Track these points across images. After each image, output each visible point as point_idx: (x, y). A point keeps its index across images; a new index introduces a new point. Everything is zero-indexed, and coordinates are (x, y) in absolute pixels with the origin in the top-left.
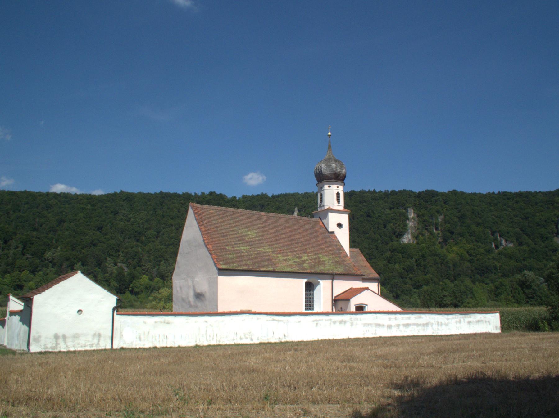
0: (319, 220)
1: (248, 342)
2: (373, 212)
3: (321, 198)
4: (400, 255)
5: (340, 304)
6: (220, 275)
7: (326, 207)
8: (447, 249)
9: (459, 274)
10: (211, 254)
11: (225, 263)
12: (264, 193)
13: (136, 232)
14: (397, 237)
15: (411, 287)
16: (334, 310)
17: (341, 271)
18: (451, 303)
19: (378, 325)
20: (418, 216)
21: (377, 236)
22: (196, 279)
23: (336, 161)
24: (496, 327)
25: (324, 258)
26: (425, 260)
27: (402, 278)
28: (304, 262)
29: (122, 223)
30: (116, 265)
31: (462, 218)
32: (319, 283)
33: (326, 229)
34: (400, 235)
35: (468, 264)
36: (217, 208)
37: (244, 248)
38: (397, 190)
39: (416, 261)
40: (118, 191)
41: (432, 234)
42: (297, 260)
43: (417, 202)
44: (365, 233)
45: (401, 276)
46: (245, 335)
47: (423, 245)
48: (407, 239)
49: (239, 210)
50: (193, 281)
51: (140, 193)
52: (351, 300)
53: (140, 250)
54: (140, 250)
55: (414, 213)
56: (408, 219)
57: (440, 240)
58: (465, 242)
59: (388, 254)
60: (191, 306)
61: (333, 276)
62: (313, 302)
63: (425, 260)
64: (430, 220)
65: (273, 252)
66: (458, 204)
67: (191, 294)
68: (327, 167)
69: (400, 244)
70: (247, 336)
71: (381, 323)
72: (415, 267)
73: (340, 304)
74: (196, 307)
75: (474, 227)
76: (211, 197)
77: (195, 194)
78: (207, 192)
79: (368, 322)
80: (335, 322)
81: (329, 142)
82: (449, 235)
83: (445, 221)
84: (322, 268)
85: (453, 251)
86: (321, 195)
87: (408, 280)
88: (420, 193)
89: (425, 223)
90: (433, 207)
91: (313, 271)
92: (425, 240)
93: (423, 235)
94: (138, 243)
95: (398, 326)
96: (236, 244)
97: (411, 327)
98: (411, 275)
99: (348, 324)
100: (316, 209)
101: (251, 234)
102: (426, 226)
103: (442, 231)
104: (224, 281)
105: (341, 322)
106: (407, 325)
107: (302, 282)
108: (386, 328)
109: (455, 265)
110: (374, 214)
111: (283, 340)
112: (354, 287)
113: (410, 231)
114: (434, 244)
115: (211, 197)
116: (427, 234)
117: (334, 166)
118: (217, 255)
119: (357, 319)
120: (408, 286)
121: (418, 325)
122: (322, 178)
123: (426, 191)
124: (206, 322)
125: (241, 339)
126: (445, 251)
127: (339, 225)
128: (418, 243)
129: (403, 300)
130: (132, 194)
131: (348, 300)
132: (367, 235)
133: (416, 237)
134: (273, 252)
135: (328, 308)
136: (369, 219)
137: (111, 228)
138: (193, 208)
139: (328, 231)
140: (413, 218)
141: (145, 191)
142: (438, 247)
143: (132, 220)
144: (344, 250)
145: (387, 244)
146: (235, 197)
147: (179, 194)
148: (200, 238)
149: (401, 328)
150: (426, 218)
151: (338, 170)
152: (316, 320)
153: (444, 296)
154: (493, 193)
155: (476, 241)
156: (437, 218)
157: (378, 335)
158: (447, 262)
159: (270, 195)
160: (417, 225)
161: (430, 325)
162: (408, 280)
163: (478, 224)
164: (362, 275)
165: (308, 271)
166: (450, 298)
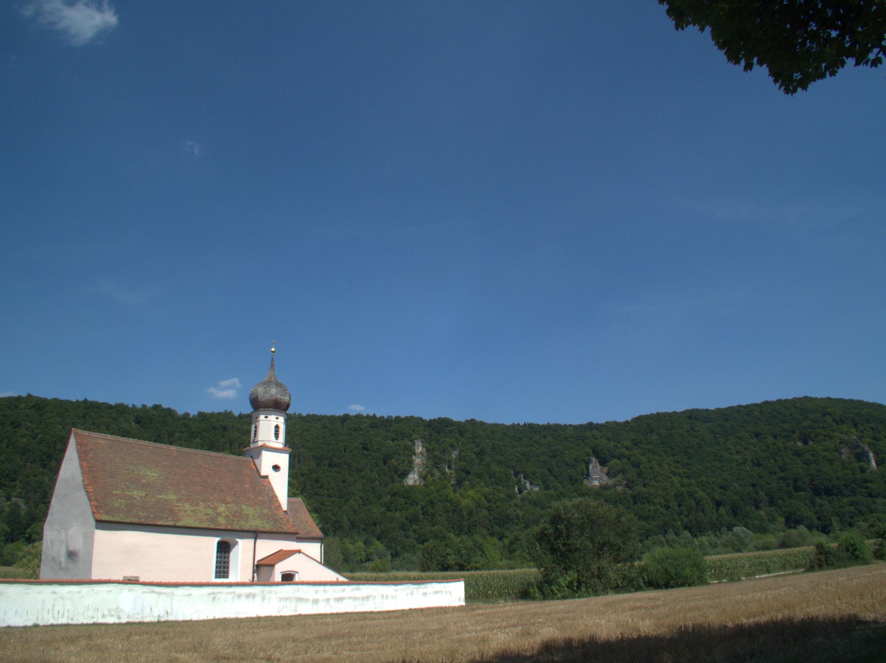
0: (250, 459)
1: (110, 620)
2: (370, 442)
3: (255, 431)
4: (402, 500)
5: (264, 570)
6: (97, 528)
7: (260, 444)
8: (461, 494)
9: (475, 526)
10: (90, 500)
11: (107, 513)
12: (228, 411)
13: (44, 454)
14: (399, 476)
15: (415, 542)
16: (256, 579)
17: (268, 527)
18: (457, 564)
19: (300, 600)
20: (428, 450)
21: (375, 475)
22: (71, 532)
23: (278, 385)
24: (459, 599)
25: (248, 510)
26: (433, 507)
27: (404, 530)
28: (219, 514)
29: (25, 440)
30: (9, 499)
31: (480, 454)
32: (237, 543)
33: (258, 471)
34: (404, 474)
35: (485, 512)
36: (109, 437)
37: (137, 494)
38: (403, 416)
39: (422, 508)
40: (24, 395)
41: (443, 473)
42: (210, 511)
43: (427, 433)
44: (359, 470)
45: (403, 528)
46: (109, 611)
47: (432, 487)
48: (412, 479)
49: (141, 442)
50: (66, 534)
51: (55, 399)
52: (276, 566)
53: (47, 480)
54: (47, 480)
55: (423, 446)
56: (415, 454)
57: (453, 482)
58: (483, 485)
59: (387, 499)
60: (61, 569)
61: (256, 534)
62: (228, 567)
63: (433, 507)
64: (442, 456)
65: (178, 501)
66: (477, 437)
67: (63, 551)
68: (266, 392)
69: (403, 486)
70: (113, 613)
71: (305, 597)
72: (421, 516)
73: (262, 569)
74: (68, 569)
75: (494, 467)
76: (155, 412)
77: (134, 406)
78: (150, 405)
79: (286, 596)
80: (239, 596)
81: (273, 360)
82: (464, 475)
83: (460, 458)
84: (243, 523)
85: (468, 496)
86: (256, 427)
87: (411, 533)
88: (430, 421)
89: (435, 460)
90: (447, 440)
91: (229, 527)
92: (434, 481)
93: (432, 475)
94: (45, 470)
95: (328, 600)
96: (127, 487)
97: (345, 602)
98: (415, 526)
99: (258, 599)
100: (249, 446)
101: (152, 475)
102: (437, 463)
103: (456, 470)
104: (102, 537)
105: (248, 596)
106: (340, 599)
107: (212, 542)
108: (310, 604)
109: (470, 514)
110: (372, 446)
111: (163, 619)
112: (285, 549)
113: (416, 469)
114: (445, 487)
115: (155, 412)
116: (437, 474)
117: (274, 391)
118: (97, 501)
119: (271, 592)
120: (410, 540)
121: (355, 599)
122: (259, 405)
123: (439, 419)
124: (55, 593)
125: (104, 616)
126: (458, 495)
127: (275, 466)
128: (425, 486)
129: (404, 559)
130: (44, 400)
131: (273, 566)
132: (362, 473)
133: (424, 478)
134: (178, 501)
135: (247, 576)
136: (365, 452)
137: (7, 447)
138: (77, 435)
139: (259, 474)
140: (421, 453)
141: (63, 397)
142: (449, 490)
143: (40, 436)
144: (277, 501)
145: (386, 485)
146: (188, 414)
147: (110, 405)
148: (79, 477)
149: (332, 602)
150: (437, 453)
151: (279, 396)
152: (213, 593)
153: (447, 554)
154: (518, 424)
155: (497, 484)
156: (450, 454)
157: (297, 613)
158: (461, 510)
159: (236, 414)
160: (425, 462)
161: (371, 599)
162: (411, 533)
163: (499, 463)
164: (296, 533)
165: (223, 527)
166: (454, 557)
